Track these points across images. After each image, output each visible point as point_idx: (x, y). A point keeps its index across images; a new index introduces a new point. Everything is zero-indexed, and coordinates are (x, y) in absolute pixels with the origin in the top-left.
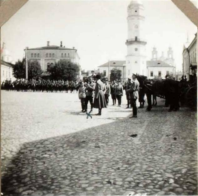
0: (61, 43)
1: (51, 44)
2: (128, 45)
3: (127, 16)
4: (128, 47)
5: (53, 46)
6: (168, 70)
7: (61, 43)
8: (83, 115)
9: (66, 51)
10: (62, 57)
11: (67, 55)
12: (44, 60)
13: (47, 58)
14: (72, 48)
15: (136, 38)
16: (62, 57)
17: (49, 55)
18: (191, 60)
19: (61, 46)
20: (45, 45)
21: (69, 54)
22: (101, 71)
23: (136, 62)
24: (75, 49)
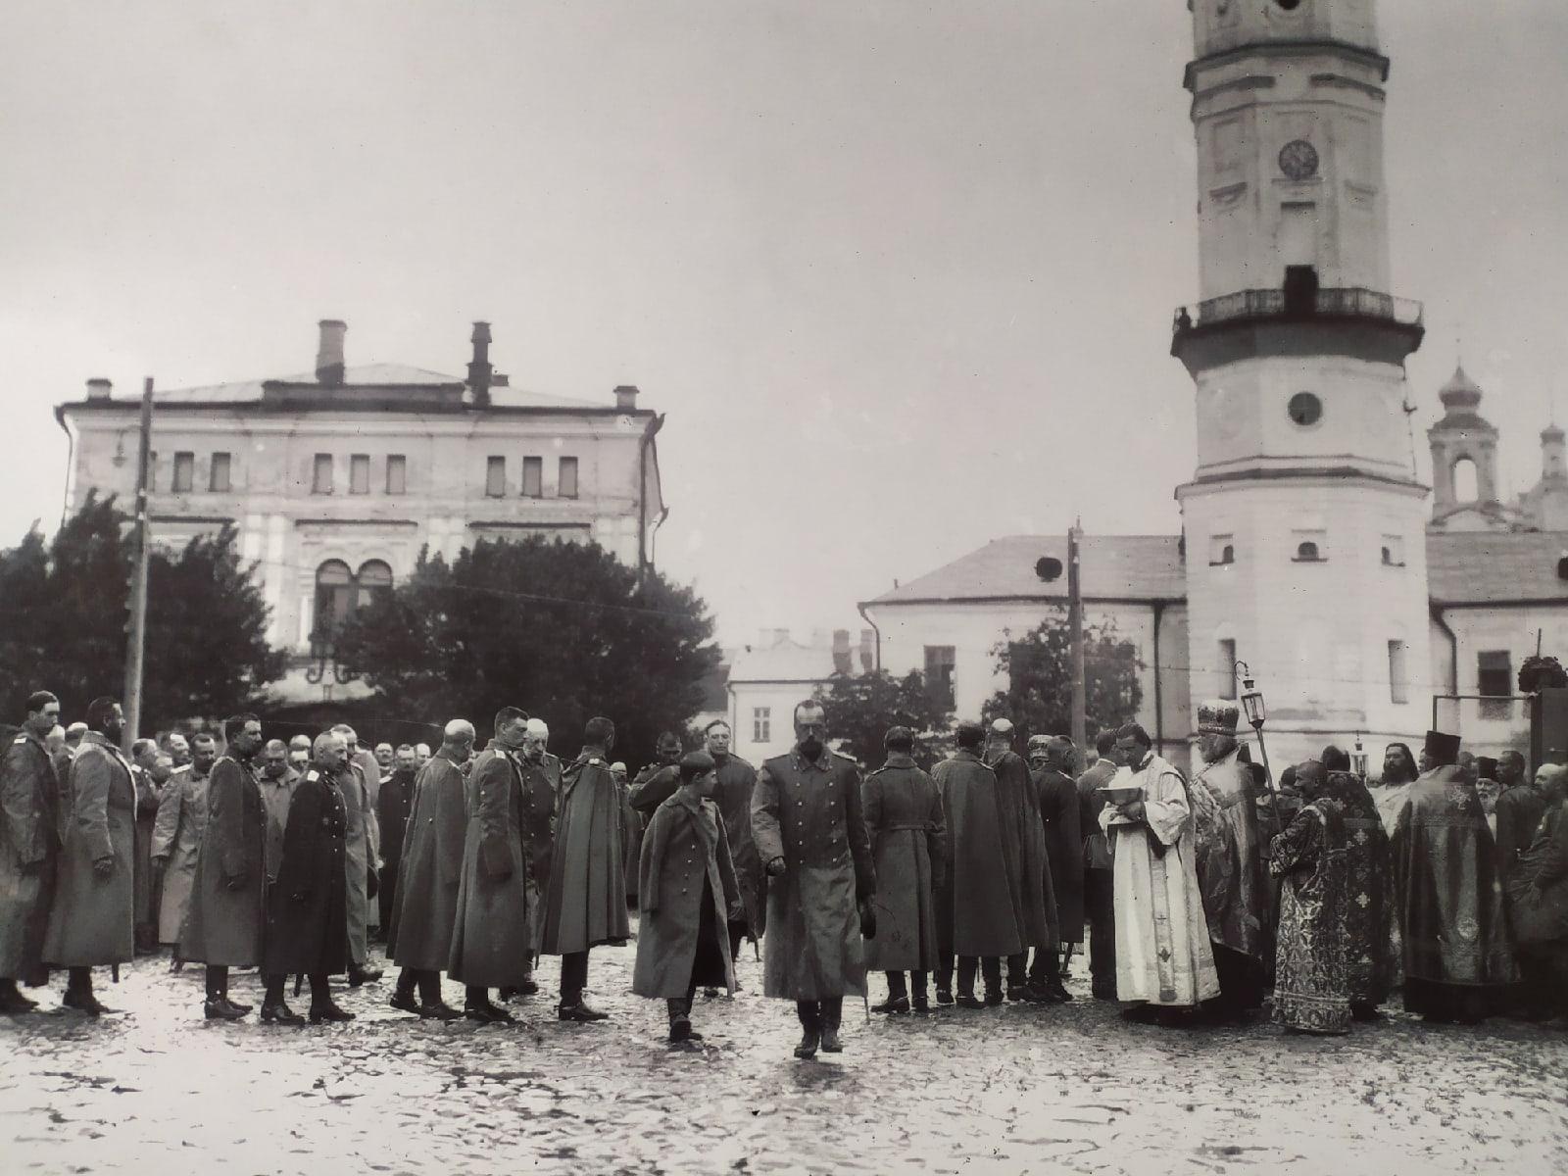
0: (481, 336)
1: (362, 365)
2: (1194, 368)
3: (1185, 52)
4: (1200, 384)
5: (1555, 615)
6: (1493, 644)
7: (481, 336)
8: (1482, 745)
9: (541, 426)
10: (494, 494)
11: (550, 473)
12: (278, 523)
13: (312, 507)
14: (611, 401)
15: (1301, 280)
16: (494, 494)
17: (340, 475)
18: (1157, 909)
19: (481, 372)
20: (300, 366)
21: (568, 461)
22: (902, 660)
23: (1308, 552)
24: (641, 403)
